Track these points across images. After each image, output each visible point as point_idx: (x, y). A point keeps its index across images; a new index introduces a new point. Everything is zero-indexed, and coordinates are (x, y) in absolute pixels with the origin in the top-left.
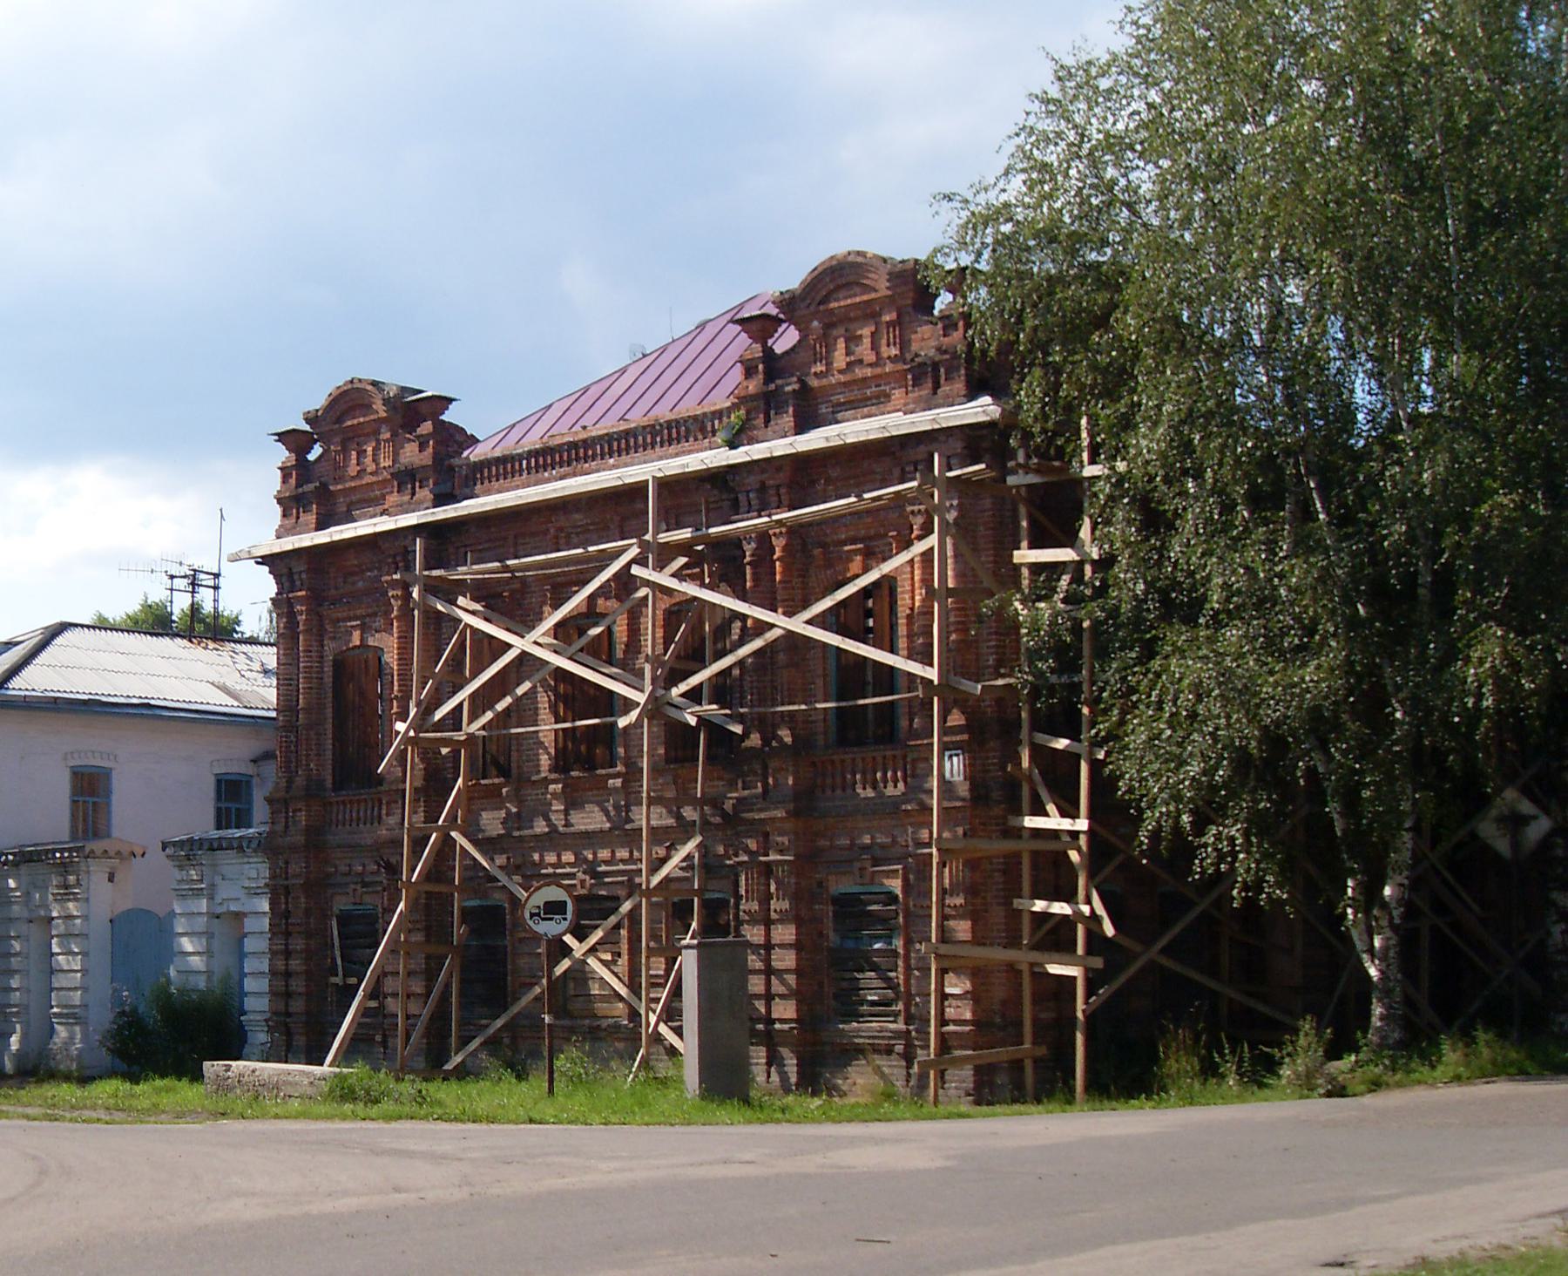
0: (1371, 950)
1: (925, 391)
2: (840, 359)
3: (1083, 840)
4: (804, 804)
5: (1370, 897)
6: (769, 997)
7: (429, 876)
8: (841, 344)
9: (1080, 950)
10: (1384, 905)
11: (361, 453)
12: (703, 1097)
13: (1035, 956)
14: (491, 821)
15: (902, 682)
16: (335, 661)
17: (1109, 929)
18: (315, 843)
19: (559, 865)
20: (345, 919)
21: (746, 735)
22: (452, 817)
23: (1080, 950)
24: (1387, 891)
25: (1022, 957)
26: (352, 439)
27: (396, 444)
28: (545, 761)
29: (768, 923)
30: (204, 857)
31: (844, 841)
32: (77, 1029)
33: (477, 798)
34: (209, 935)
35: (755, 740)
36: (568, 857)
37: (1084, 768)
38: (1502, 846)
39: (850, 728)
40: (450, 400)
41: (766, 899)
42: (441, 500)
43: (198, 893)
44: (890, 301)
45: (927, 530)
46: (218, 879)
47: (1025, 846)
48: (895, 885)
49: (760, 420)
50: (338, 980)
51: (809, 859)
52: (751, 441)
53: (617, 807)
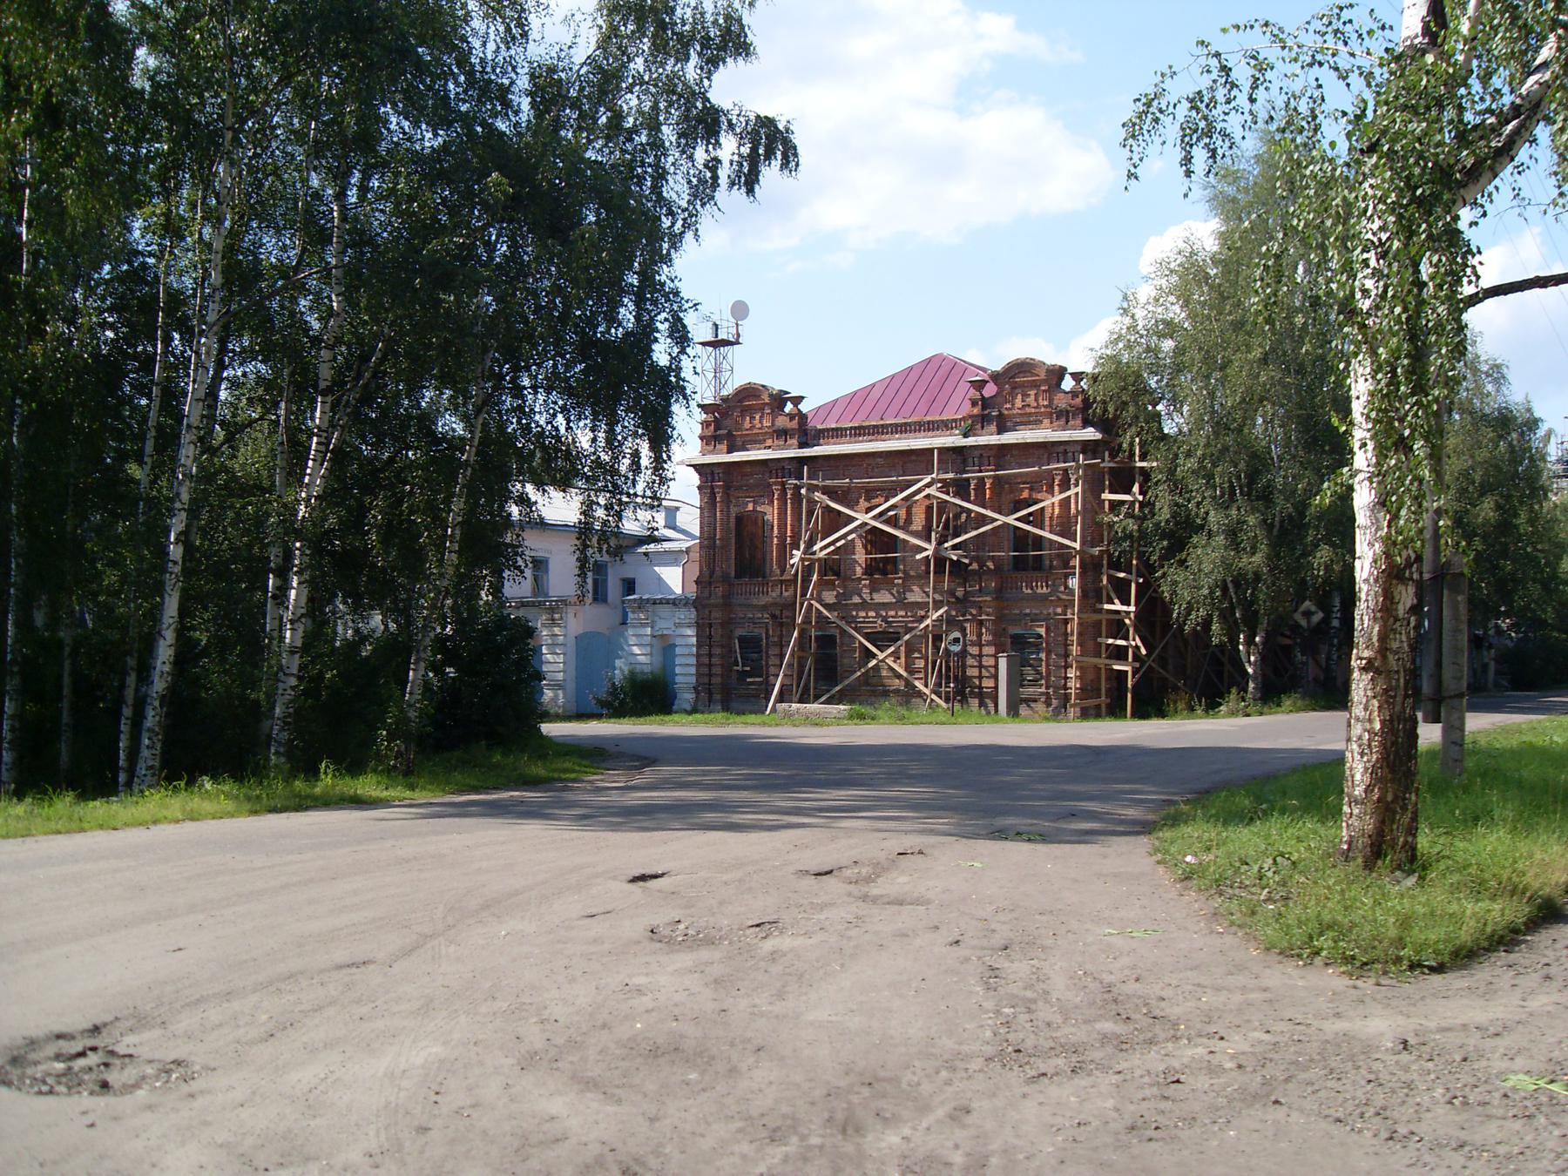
0: (1249, 661)
1: (1062, 422)
2: (1018, 402)
3: (1132, 615)
4: (999, 594)
5: (1250, 642)
6: (980, 677)
7: (803, 622)
8: (1019, 397)
9: (1130, 659)
10: (1256, 645)
11: (752, 418)
12: (1008, 714)
13: (1108, 661)
14: (830, 597)
15: (1046, 545)
16: (737, 517)
17: (1143, 651)
18: (727, 604)
19: (867, 617)
20: (742, 639)
21: (970, 564)
22: (812, 595)
23: (1130, 659)
24: (1257, 639)
25: (1102, 662)
26: (748, 411)
27: (774, 416)
28: (859, 570)
29: (981, 646)
30: (650, 608)
31: (1017, 612)
32: (560, 692)
33: (822, 584)
34: (651, 645)
35: (975, 566)
36: (872, 614)
37: (1133, 586)
38: (1304, 623)
39: (1020, 564)
40: (803, 398)
41: (980, 635)
42: (802, 445)
43: (644, 625)
44: (1045, 381)
45: (1076, 485)
46: (656, 619)
47: (1103, 617)
48: (1042, 631)
49: (979, 426)
50: (739, 668)
51: (1000, 618)
52: (974, 435)
53: (898, 592)
